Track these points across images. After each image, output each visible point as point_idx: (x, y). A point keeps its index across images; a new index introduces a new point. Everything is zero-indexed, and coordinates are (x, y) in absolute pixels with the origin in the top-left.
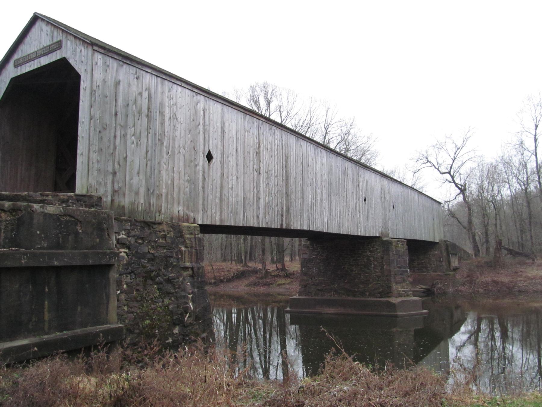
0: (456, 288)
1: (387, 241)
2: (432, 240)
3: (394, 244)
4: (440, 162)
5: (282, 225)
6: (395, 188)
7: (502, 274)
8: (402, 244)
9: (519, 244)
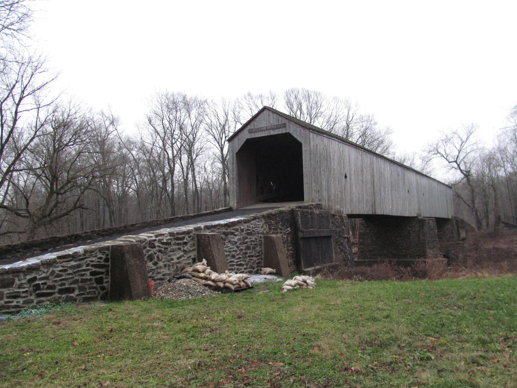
0: (465, 254)
1: (421, 219)
2: (447, 217)
3: (427, 221)
4: (448, 152)
5: (373, 212)
6: (424, 181)
7: (501, 242)
8: (433, 221)
9: (513, 219)
